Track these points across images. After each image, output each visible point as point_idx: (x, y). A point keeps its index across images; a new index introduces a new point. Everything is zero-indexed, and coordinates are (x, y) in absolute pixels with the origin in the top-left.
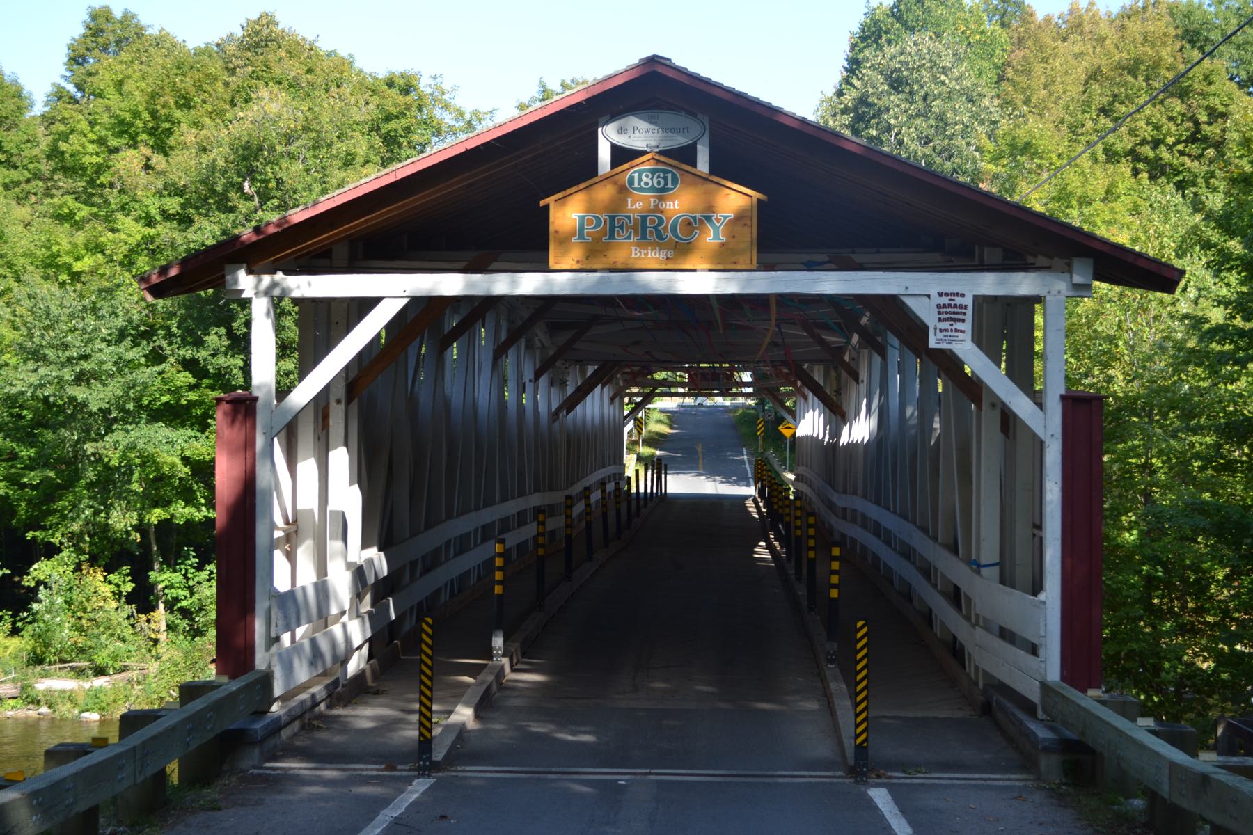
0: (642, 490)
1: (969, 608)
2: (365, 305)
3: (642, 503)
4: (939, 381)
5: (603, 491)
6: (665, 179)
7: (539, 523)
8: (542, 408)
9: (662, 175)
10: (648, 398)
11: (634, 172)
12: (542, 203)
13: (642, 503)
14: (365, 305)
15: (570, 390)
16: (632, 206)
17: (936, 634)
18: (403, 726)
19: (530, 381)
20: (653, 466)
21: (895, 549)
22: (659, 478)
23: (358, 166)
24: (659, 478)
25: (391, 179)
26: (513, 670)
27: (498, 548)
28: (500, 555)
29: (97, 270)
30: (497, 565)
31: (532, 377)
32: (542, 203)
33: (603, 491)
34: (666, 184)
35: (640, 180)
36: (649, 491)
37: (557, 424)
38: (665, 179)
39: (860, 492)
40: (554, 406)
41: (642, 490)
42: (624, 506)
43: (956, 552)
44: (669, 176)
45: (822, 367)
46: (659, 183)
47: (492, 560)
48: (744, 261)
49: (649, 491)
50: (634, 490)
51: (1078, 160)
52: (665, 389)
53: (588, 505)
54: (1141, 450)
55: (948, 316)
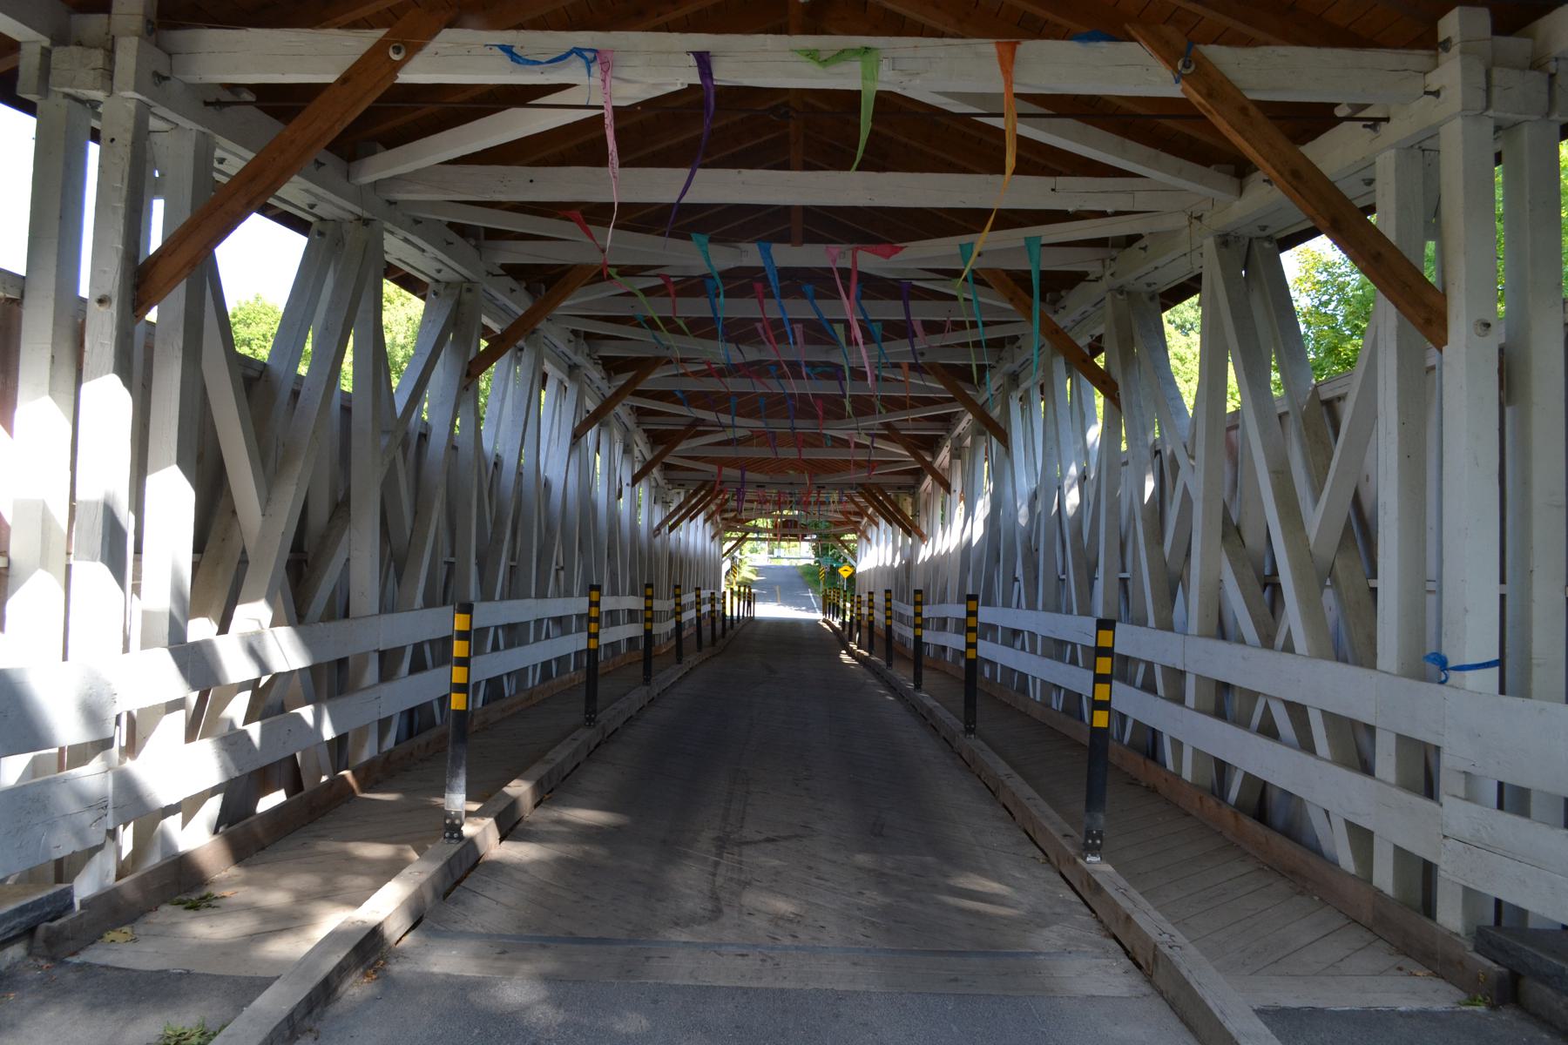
0: (735, 614)
3: (728, 624)
5: (698, 611)
7: (591, 636)
8: (642, 519)
10: (742, 540)
13: (728, 624)
15: (672, 509)
19: (628, 485)
20: (744, 597)
22: (749, 605)
23: (1015, 346)
24: (749, 605)
26: (364, 791)
27: (461, 622)
28: (463, 635)
29: (774, 501)
30: (455, 654)
31: (630, 482)
33: (698, 611)
36: (741, 615)
37: (658, 539)
40: (657, 522)
41: (735, 614)
42: (719, 625)
47: (447, 642)
48: (1423, 793)
49: (741, 615)
50: (728, 613)
51: (736, 429)
52: (755, 536)
53: (679, 624)
54: (733, 504)
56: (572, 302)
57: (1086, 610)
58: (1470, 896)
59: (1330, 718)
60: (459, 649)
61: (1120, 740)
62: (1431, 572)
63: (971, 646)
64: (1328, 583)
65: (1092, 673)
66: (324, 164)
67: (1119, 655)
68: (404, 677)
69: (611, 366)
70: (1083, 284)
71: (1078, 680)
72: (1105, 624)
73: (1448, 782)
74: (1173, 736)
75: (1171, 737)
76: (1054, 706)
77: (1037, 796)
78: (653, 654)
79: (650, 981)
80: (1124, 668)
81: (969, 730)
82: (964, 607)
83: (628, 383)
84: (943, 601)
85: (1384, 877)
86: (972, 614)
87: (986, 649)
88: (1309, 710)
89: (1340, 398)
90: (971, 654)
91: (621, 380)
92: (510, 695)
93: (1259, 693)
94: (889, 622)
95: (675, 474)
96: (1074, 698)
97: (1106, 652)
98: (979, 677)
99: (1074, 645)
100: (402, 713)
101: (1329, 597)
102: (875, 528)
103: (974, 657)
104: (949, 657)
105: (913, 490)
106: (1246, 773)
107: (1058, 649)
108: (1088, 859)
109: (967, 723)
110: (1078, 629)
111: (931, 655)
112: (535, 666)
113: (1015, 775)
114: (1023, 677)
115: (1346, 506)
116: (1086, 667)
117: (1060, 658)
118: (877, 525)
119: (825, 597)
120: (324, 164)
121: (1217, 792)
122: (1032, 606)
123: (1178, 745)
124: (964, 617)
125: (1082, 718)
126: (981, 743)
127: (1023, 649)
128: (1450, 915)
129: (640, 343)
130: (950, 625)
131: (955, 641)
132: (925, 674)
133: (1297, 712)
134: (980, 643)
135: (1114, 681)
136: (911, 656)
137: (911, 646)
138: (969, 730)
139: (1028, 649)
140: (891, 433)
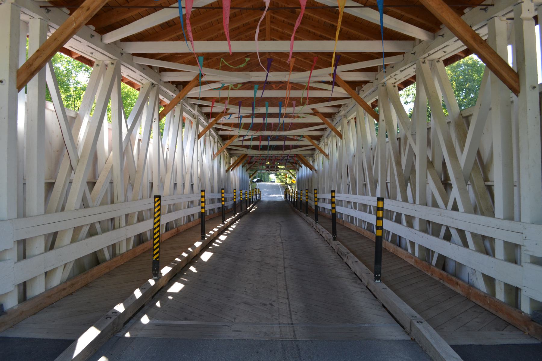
55: (254, 197)
56: (195, 92)
57: (373, 195)
58: (532, 301)
59: (474, 235)
60: (223, 199)
61: (387, 240)
62: (515, 179)
63: (334, 208)
64: (469, 183)
65: (376, 216)
66: (94, 36)
67: (387, 210)
68: (124, 227)
69: (208, 116)
70: (368, 84)
71: (372, 219)
72: (379, 199)
73: (525, 258)
74: (411, 240)
75: (410, 241)
76: (363, 227)
77: (387, 287)
78: (206, 220)
79: (220, 339)
80: (389, 215)
81: (335, 239)
82: (330, 195)
83: (214, 121)
84: (324, 193)
85: (500, 295)
86: (333, 197)
87: (389, 225)
88: (465, 231)
89: (471, 115)
90: (334, 211)
91: (212, 120)
92: (184, 224)
93: (442, 225)
94: (307, 200)
95: (232, 152)
96: (370, 225)
97: (302, 193)
98: (336, 218)
99: (370, 206)
100: (135, 236)
101: (470, 188)
102: (301, 168)
103: (335, 212)
104: (326, 211)
105: (312, 156)
106: (392, 233)
107: (364, 207)
108: (376, 281)
109: (376, 273)
110: (372, 201)
111: (320, 210)
112: (184, 217)
113: (359, 262)
114: (352, 217)
115: (475, 155)
116: (374, 214)
117: (365, 211)
118: (301, 167)
119: (285, 192)
120: (94, 36)
121: (427, 260)
122: (354, 193)
123: (356, 218)
124: (331, 198)
125: (374, 233)
126: (384, 286)
127: (352, 208)
128: (526, 308)
129: (218, 108)
130: (327, 201)
131: (329, 206)
132: (319, 218)
133: (461, 233)
134: (337, 207)
135: (384, 219)
136: (314, 211)
137: (314, 208)
138: (335, 239)
139: (353, 208)
140: (315, 113)
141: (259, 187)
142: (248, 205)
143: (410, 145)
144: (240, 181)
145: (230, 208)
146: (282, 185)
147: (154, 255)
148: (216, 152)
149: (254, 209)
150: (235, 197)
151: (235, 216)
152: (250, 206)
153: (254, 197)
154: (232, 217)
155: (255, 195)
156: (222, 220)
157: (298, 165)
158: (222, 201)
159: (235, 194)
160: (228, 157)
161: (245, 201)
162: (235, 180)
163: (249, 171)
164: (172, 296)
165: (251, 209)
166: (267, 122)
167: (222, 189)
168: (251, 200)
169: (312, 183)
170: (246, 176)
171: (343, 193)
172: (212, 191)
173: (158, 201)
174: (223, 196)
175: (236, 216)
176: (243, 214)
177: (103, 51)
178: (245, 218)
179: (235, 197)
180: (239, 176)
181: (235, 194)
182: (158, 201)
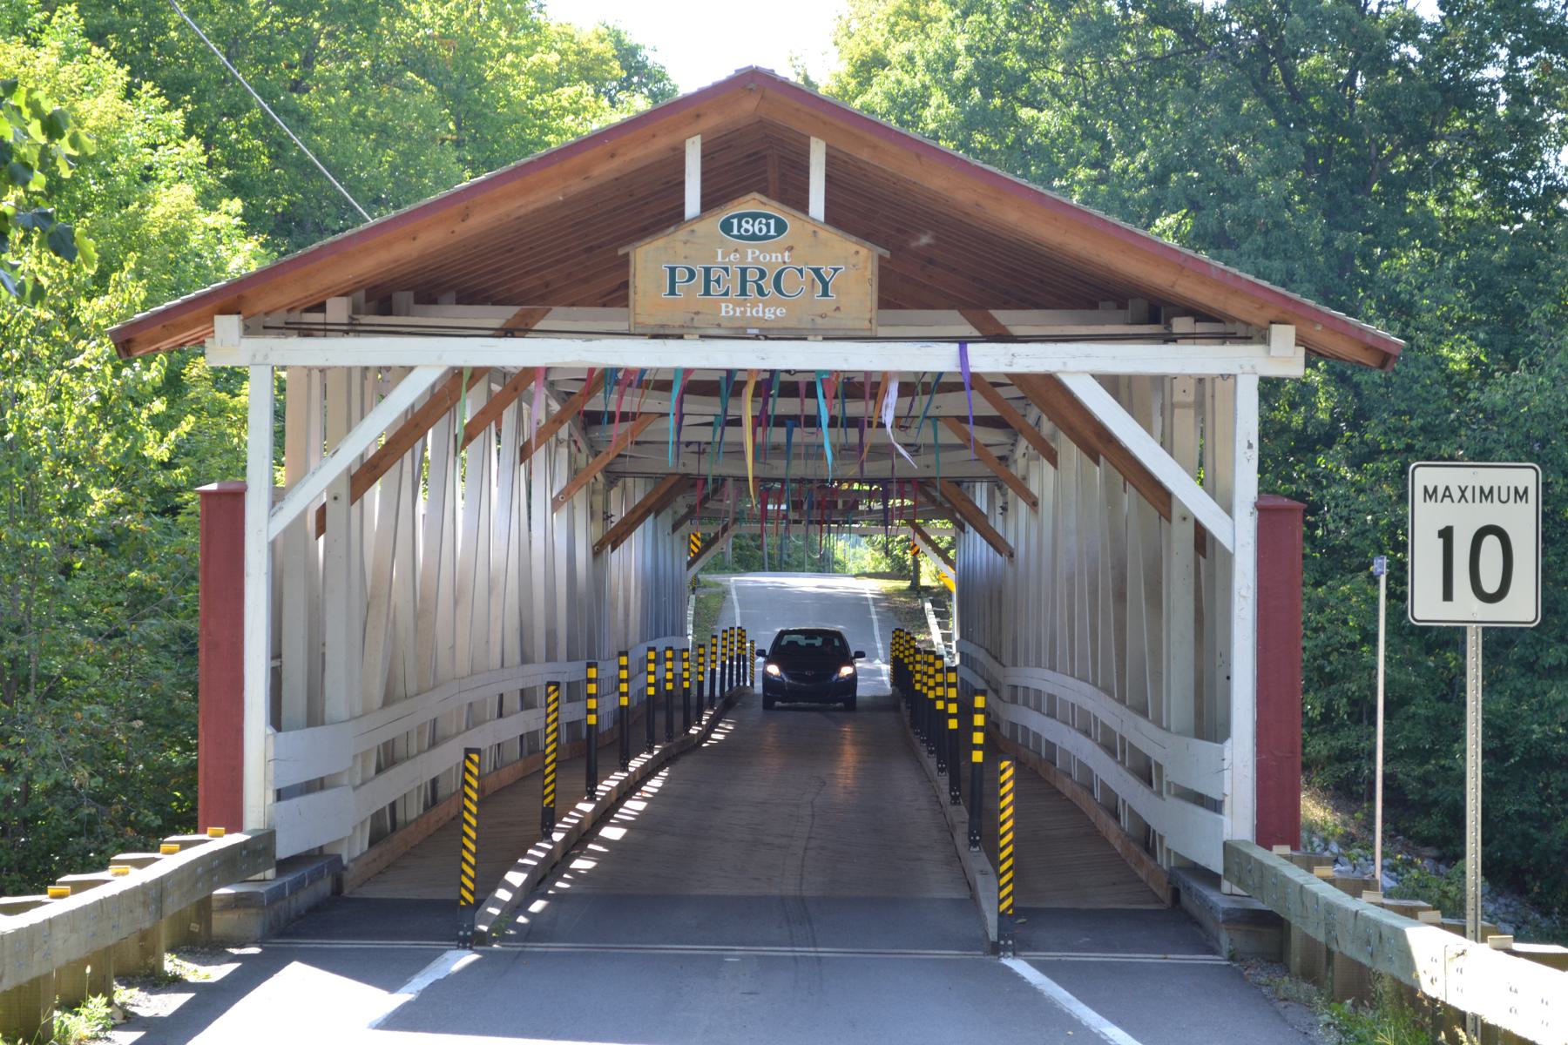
1: (1160, 777)
2: (1113, 384)
4: (1011, 962)
6: (768, 225)
9: (764, 221)
11: (733, 217)
12: (621, 252)
14: (1113, 384)
16: (723, 258)
17: (1161, 866)
18: (931, 763)
21: (1095, 740)
25: (1238, 438)
32: (621, 252)
34: (768, 231)
35: (740, 226)
38: (768, 225)
39: (1044, 708)
43: (1150, 783)
44: (772, 222)
45: (985, 485)
46: (760, 230)
55: (718, 676)
102: (1048, 467)
141: (743, 620)
142: (693, 713)
143: (1229, 510)
144: (645, 591)
145: (606, 728)
146: (887, 596)
147: (545, 797)
148: (564, 483)
149: (721, 737)
150: (624, 674)
151: (650, 752)
152: (700, 721)
153: (718, 676)
154: (580, 806)
155: (723, 663)
156: (621, 758)
157: (1023, 443)
158: (590, 696)
159: (624, 661)
160: (600, 486)
161: (681, 693)
162: (626, 590)
163: (686, 528)
164: (519, 924)
165: (705, 735)
166: (776, 413)
167: (621, 654)
168: (707, 693)
169: (1000, 612)
170: (676, 554)
171: (1471, 628)
172: (551, 656)
173: (554, 691)
174: (594, 676)
175: (656, 752)
176: (675, 751)
177: (1078, 1012)
178: (687, 763)
179: (624, 674)
180: (640, 563)
181: (624, 661)
182: (554, 691)
